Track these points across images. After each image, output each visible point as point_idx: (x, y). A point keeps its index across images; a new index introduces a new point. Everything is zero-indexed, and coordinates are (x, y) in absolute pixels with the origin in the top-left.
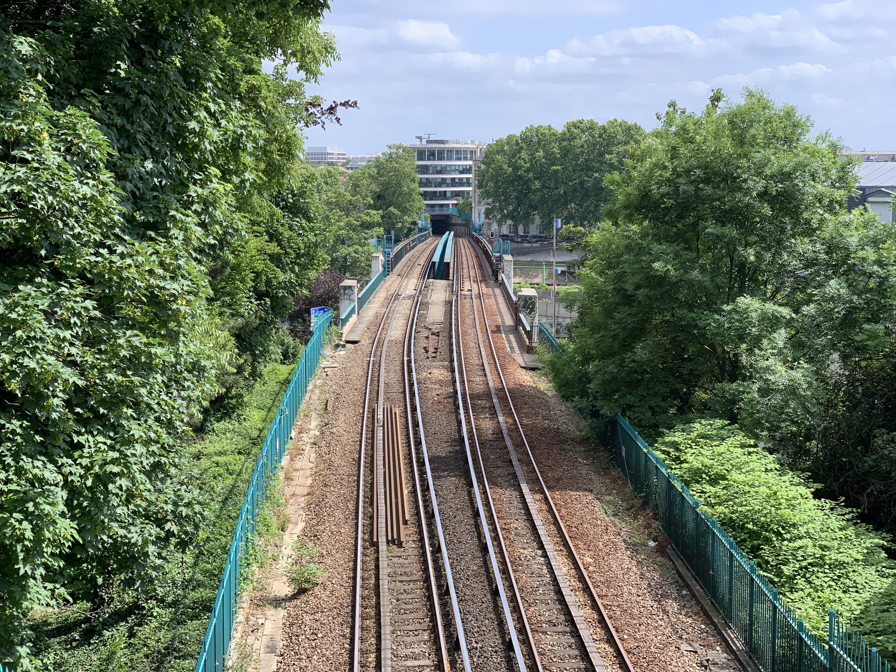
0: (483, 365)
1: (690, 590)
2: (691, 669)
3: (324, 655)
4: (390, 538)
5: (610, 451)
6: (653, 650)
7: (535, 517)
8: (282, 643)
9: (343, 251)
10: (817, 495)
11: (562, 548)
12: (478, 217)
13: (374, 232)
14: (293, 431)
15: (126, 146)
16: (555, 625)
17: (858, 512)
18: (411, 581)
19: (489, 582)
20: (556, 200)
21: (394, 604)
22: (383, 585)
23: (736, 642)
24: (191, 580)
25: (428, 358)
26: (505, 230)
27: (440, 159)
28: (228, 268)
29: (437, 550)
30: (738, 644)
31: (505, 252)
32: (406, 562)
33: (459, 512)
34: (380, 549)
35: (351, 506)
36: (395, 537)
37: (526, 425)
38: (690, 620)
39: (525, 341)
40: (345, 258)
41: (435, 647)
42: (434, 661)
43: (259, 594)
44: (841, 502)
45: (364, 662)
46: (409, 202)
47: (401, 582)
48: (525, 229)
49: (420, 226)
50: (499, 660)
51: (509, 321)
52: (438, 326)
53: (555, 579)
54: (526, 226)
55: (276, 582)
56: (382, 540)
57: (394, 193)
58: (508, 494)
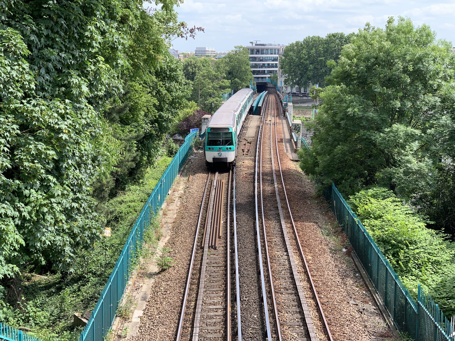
0: (271, 159)
1: (360, 274)
3: (169, 302)
4: (210, 245)
5: (329, 203)
6: (335, 303)
7: (285, 236)
8: (150, 296)
12: (281, 82)
13: (226, 91)
14: (170, 191)
16: (287, 290)
17: (450, 236)
18: (218, 267)
19: (257, 268)
20: (321, 75)
21: (208, 278)
22: (203, 268)
24: (109, 263)
25: (244, 155)
26: (294, 90)
27: (262, 54)
29: (233, 252)
30: (380, 301)
32: (217, 257)
33: (248, 233)
34: (204, 250)
35: (193, 229)
36: (213, 244)
38: (357, 289)
39: (294, 147)
40: (211, 104)
41: (225, 300)
42: (223, 306)
43: (143, 271)
44: (443, 231)
45: (189, 306)
46: (245, 76)
47: (213, 267)
48: (304, 90)
51: (288, 136)
54: (305, 88)
55: (151, 266)
56: (206, 246)
57: (238, 71)
58: (273, 224)
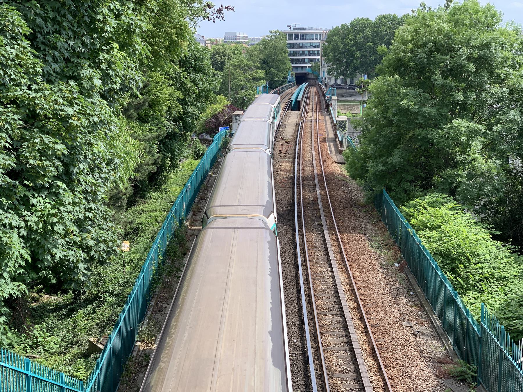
1: (415, 292)
2: (407, 337)
5: (379, 211)
6: (386, 325)
7: (329, 249)
9: (242, 94)
10: (494, 237)
11: (343, 267)
12: (323, 73)
13: (260, 83)
15: (58, 29)
16: (332, 311)
17: (518, 248)
23: (437, 321)
24: (128, 281)
25: (281, 156)
26: (339, 82)
28: (147, 103)
31: (333, 95)
37: (332, 196)
38: (412, 309)
40: (243, 98)
44: (510, 242)
48: (351, 81)
49: (288, 79)
50: (296, 329)
51: (331, 135)
52: (290, 138)
53: (336, 285)
54: (352, 79)
57: (274, 59)
58: (316, 235)
